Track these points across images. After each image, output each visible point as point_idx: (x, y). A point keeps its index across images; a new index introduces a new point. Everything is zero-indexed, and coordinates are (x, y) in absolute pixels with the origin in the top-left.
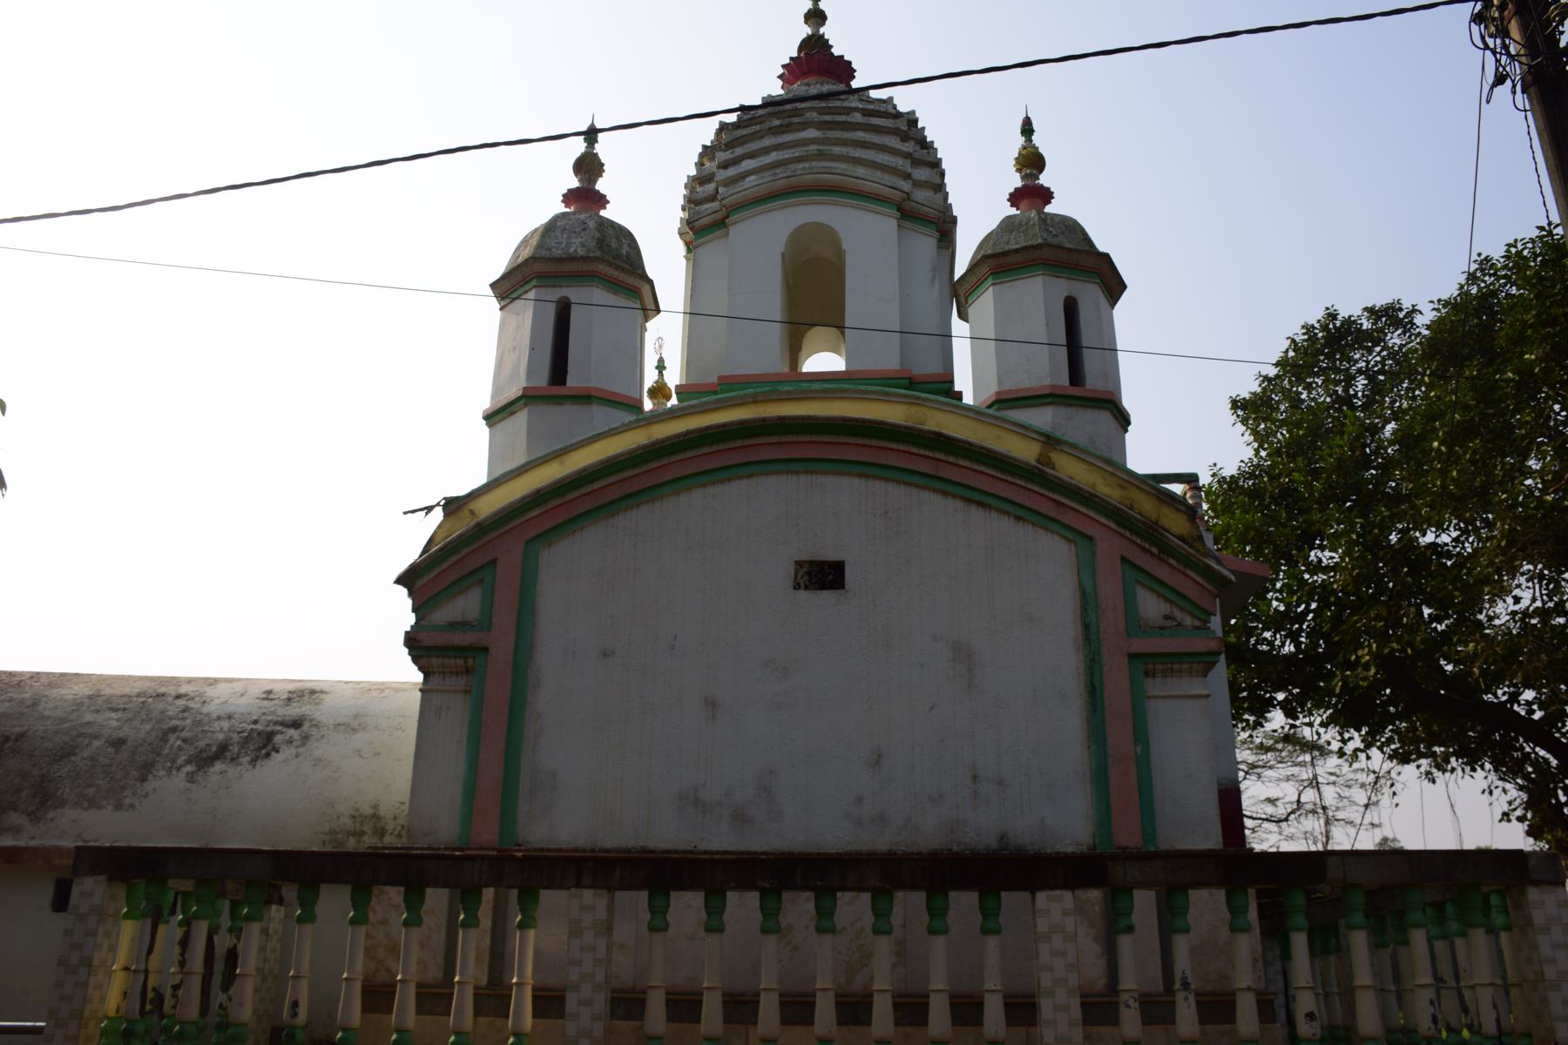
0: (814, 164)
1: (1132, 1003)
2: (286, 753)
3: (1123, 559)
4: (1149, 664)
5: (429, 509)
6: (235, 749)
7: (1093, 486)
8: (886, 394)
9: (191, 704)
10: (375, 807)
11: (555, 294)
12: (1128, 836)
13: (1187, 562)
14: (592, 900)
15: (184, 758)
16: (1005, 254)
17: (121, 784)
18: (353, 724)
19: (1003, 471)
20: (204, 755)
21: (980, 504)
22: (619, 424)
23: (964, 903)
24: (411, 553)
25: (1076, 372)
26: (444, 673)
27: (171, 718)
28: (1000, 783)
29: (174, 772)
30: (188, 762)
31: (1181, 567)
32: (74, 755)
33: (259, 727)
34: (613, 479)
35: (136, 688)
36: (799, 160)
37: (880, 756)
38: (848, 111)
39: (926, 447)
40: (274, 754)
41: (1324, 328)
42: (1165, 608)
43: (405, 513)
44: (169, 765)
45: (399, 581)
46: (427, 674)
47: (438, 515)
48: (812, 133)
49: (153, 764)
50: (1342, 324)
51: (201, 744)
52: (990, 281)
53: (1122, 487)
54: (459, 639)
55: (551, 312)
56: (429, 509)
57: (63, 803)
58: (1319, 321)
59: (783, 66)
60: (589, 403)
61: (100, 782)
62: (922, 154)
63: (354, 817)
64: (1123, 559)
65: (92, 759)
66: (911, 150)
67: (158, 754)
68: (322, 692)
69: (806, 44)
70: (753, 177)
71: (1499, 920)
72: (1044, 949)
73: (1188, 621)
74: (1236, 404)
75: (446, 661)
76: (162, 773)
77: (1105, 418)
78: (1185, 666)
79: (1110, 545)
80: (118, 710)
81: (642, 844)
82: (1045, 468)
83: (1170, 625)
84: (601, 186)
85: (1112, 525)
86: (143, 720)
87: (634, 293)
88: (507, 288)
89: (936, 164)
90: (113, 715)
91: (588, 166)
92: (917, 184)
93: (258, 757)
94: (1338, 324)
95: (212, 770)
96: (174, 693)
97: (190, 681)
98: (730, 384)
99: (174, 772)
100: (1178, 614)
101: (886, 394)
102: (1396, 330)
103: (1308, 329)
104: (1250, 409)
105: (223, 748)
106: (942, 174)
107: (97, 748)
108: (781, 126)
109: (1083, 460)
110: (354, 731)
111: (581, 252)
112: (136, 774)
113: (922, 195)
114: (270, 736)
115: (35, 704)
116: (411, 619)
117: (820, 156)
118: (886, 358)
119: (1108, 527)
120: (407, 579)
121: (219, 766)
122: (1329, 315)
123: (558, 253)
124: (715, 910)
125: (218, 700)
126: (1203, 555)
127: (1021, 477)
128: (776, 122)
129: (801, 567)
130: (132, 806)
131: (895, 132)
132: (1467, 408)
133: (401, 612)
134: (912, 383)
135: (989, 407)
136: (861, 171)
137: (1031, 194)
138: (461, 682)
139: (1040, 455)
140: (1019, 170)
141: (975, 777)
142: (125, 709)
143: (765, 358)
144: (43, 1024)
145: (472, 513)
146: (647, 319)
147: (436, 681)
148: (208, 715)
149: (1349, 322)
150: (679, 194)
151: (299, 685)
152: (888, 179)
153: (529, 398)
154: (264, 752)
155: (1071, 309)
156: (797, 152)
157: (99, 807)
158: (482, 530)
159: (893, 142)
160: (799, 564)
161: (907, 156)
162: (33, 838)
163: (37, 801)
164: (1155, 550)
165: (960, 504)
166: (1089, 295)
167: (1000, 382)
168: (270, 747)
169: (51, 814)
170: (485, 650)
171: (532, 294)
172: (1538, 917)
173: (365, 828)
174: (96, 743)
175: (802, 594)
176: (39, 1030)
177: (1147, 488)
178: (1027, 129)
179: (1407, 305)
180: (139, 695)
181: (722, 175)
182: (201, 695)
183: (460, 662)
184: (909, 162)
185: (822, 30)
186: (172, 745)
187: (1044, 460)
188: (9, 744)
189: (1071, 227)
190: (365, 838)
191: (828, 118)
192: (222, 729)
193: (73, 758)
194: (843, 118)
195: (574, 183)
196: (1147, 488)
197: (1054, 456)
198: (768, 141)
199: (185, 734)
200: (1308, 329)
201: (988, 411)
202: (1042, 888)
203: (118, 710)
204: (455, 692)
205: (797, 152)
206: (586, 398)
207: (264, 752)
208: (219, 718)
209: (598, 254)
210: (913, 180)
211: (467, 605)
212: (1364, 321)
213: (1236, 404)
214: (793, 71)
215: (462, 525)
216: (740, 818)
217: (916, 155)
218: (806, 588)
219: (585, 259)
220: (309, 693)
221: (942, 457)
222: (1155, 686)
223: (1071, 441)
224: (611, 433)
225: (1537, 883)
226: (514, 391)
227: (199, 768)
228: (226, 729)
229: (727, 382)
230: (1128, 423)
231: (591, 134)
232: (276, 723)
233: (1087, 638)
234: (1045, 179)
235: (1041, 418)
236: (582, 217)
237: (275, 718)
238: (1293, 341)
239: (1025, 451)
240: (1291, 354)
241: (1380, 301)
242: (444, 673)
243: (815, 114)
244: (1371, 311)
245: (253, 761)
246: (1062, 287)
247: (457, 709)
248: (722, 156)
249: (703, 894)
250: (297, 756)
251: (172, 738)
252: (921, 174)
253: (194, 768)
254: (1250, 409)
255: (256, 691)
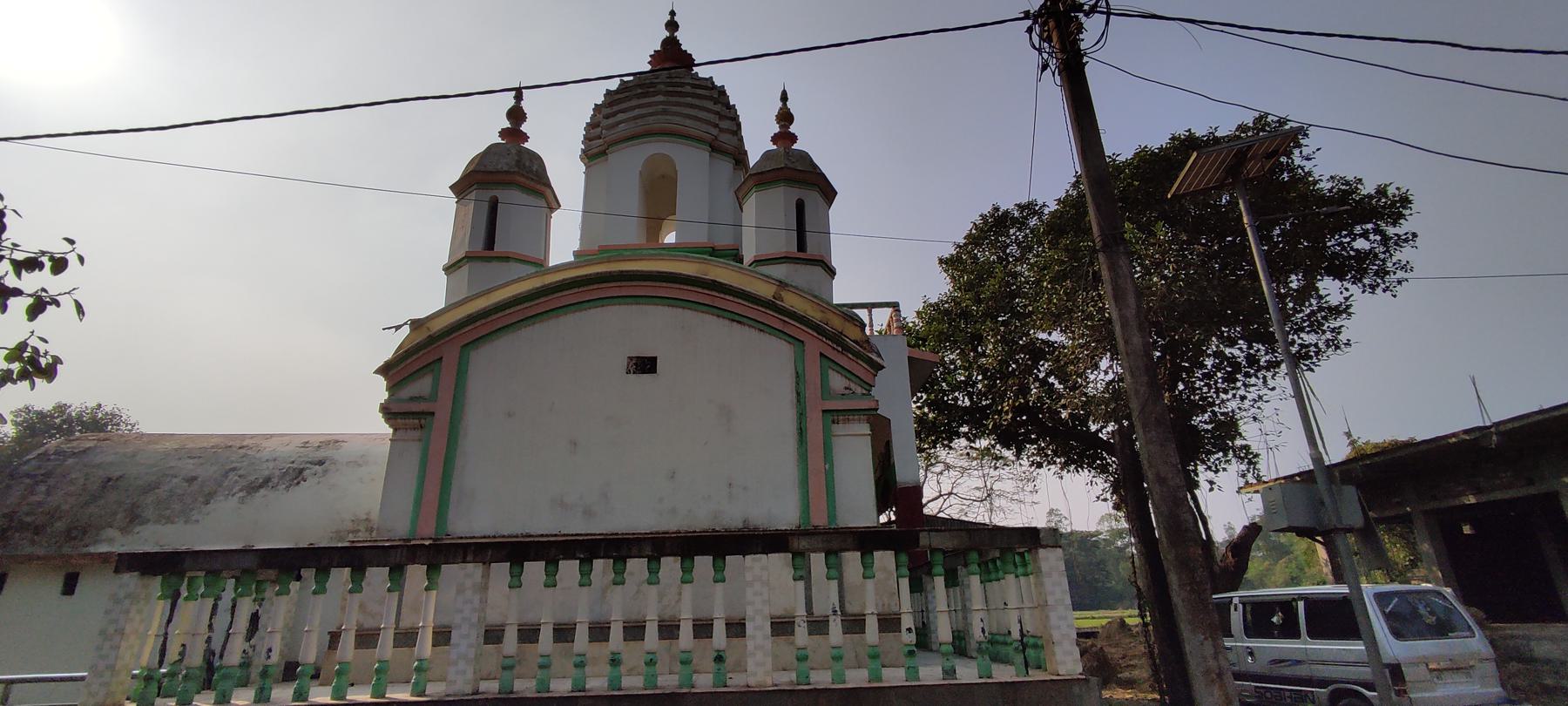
0: (659, 117)
1: (802, 623)
2: (311, 481)
3: (821, 354)
4: (834, 416)
5: (398, 328)
6: (276, 480)
7: (805, 312)
8: (686, 256)
9: (250, 452)
10: (368, 514)
11: (488, 194)
12: (819, 520)
13: (857, 355)
14: (473, 571)
15: (237, 488)
16: (762, 173)
17: (191, 507)
18: (358, 462)
19: (752, 302)
20: (253, 485)
21: (739, 322)
22: (525, 274)
23: (703, 563)
24: (387, 354)
25: (802, 246)
26: (406, 429)
27: (232, 462)
28: (745, 488)
29: (230, 497)
30: (241, 490)
31: (854, 358)
32: (158, 488)
33: (295, 465)
34: (519, 308)
35: (213, 442)
36: (651, 114)
37: (674, 473)
38: (682, 85)
39: (708, 289)
40: (302, 482)
41: (992, 216)
42: (845, 383)
43: (384, 329)
44: (227, 493)
45: (377, 372)
46: (395, 430)
47: (406, 330)
48: (660, 98)
49: (215, 492)
50: (1003, 214)
51: (252, 478)
52: (754, 189)
53: (822, 311)
54: (415, 407)
55: (485, 207)
56: (398, 328)
57: (146, 522)
58: (989, 212)
59: (651, 56)
60: (508, 262)
61: (176, 506)
62: (725, 111)
63: (353, 521)
64: (821, 354)
65: (171, 491)
66: (719, 110)
67: (220, 486)
68: (343, 441)
69: (665, 42)
70: (623, 125)
71: (1020, 570)
72: (749, 592)
73: (859, 390)
74: (941, 261)
75: (407, 421)
76: (222, 498)
77: (818, 270)
78: (856, 417)
79: (814, 346)
80: (195, 457)
81: (527, 531)
82: (777, 302)
83: (847, 394)
84: (524, 128)
85: (815, 334)
86: (212, 464)
87: (541, 194)
88: (460, 189)
89: (735, 119)
90: (191, 461)
91: (517, 115)
92: (721, 130)
93: (291, 485)
94: (1000, 213)
95: (257, 494)
96: (238, 445)
97: (253, 436)
98: (607, 253)
99: (230, 497)
100: (853, 386)
101: (686, 256)
102: (1034, 216)
103: (983, 217)
104: (948, 263)
105: (267, 480)
106: (739, 125)
107: (176, 483)
108: (642, 93)
109: (801, 296)
110: (360, 465)
111: (505, 168)
112: (201, 499)
113: (725, 137)
114: (301, 471)
115: (134, 455)
116: (386, 395)
117: (665, 112)
118: (700, 236)
119: (812, 335)
120: (385, 370)
121: (262, 491)
122: (995, 208)
123: (490, 168)
124: (586, 573)
125: (269, 445)
126: (869, 352)
127: (762, 306)
128: (640, 91)
129: (631, 360)
130: (197, 521)
131: (710, 98)
132: (1063, 262)
133: (379, 390)
134: (714, 252)
135: (750, 266)
136: (688, 122)
137: (785, 137)
138: (417, 434)
139: (775, 293)
140: (778, 123)
141: (730, 485)
142: (200, 457)
143: (630, 233)
144: (86, 674)
145: (428, 329)
146: (552, 212)
147: (401, 433)
148: (260, 459)
149: (1007, 213)
150: (581, 133)
151: (329, 438)
152: (705, 127)
153: (469, 258)
154: (295, 481)
155: (800, 206)
156: (651, 110)
157: (172, 523)
158: (432, 340)
159: (709, 104)
160: (631, 358)
161: (717, 113)
162: (123, 545)
163: (128, 520)
164: (840, 349)
165: (727, 322)
166: (812, 198)
167: (757, 249)
168: (300, 478)
169: (138, 529)
170: (433, 414)
171: (473, 196)
172: (1045, 567)
173: (359, 528)
174: (175, 480)
175: (632, 376)
176: (82, 679)
177: (838, 312)
178: (784, 98)
179: (1040, 202)
180: (213, 447)
181: (605, 122)
182: (257, 446)
183: (416, 421)
184: (717, 116)
185: (676, 34)
186: (232, 479)
187: (777, 296)
188: (110, 483)
189: (805, 157)
190: (360, 534)
191: (671, 89)
192: (268, 468)
193: (157, 491)
194: (679, 89)
195: (507, 124)
196: (838, 312)
197: (783, 293)
198: (634, 103)
199: (241, 472)
200: (983, 217)
201: (750, 268)
202: (748, 554)
203: (195, 457)
204: (413, 440)
205: (651, 110)
206: (506, 258)
207: (295, 481)
208: (267, 460)
209: (516, 169)
210: (720, 128)
211: (423, 386)
212: (1015, 212)
213: (941, 261)
214: (656, 58)
215: (422, 336)
216: (588, 513)
217: (723, 113)
218: (634, 373)
219: (507, 172)
220: (334, 442)
221: (717, 294)
222: (839, 429)
223: (794, 284)
224: (529, 277)
225: (1045, 547)
226: (461, 254)
227: (249, 493)
228: (271, 468)
229: (603, 249)
230: (835, 274)
231: (519, 93)
232: (308, 462)
233: (798, 401)
234: (793, 129)
235: (779, 271)
236: (508, 146)
237: (306, 459)
238: (975, 224)
239: (765, 291)
240: (974, 231)
241: (1024, 201)
242: (406, 429)
243: (663, 87)
244: (1018, 205)
245: (288, 488)
246: (796, 193)
247: (413, 452)
248: (608, 111)
249: (544, 563)
250: (319, 483)
251: (231, 475)
252: (725, 124)
253: (245, 494)
254: (948, 263)
255: (298, 442)
